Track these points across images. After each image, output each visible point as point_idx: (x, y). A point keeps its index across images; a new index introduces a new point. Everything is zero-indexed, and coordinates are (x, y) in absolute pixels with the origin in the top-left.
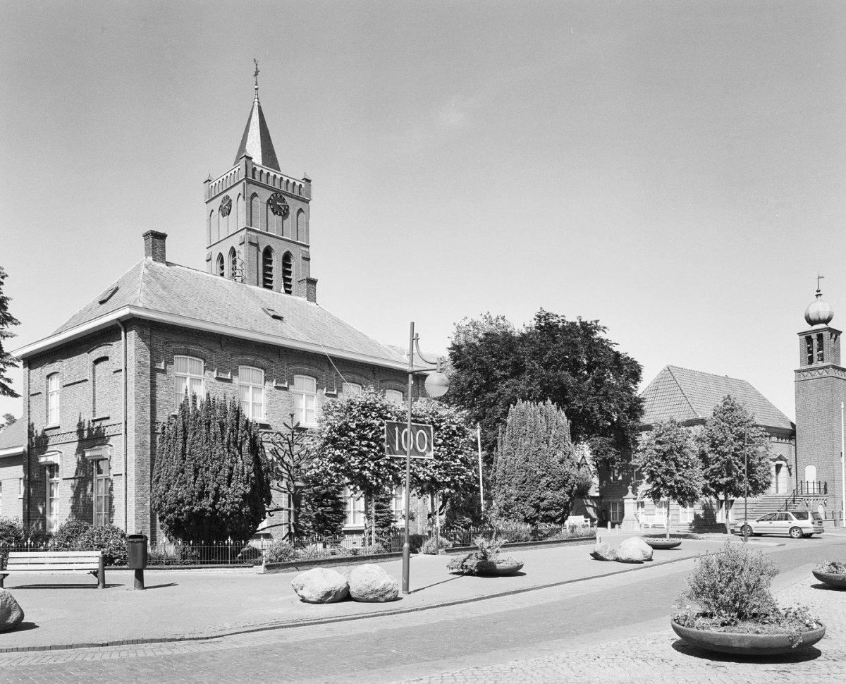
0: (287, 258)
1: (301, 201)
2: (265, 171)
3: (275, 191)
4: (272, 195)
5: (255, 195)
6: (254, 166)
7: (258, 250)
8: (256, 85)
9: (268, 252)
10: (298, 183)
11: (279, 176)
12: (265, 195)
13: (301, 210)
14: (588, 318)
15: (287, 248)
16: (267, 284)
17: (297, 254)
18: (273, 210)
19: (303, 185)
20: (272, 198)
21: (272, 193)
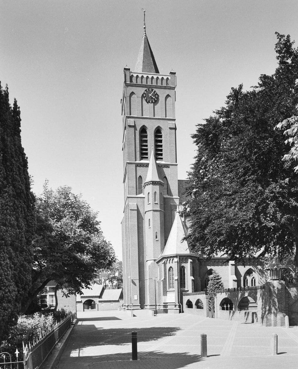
0: (158, 131)
1: (169, 89)
2: (145, 76)
3: (147, 87)
4: (146, 90)
5: (133, 93)
6: (132, 74)
7: (135, 129)
8: (145, 25)
9: (143, 130)
10: (165, 78)
11: (160, 77)
12: (140, 91)
13: (168, 96)
14: (229, 92)
15: (156, 124)
16: (144, 152)
17: (165, 127)
18: (146, 100)
19: (169, 78)
20: (145, 92)
21: (146, 89)
